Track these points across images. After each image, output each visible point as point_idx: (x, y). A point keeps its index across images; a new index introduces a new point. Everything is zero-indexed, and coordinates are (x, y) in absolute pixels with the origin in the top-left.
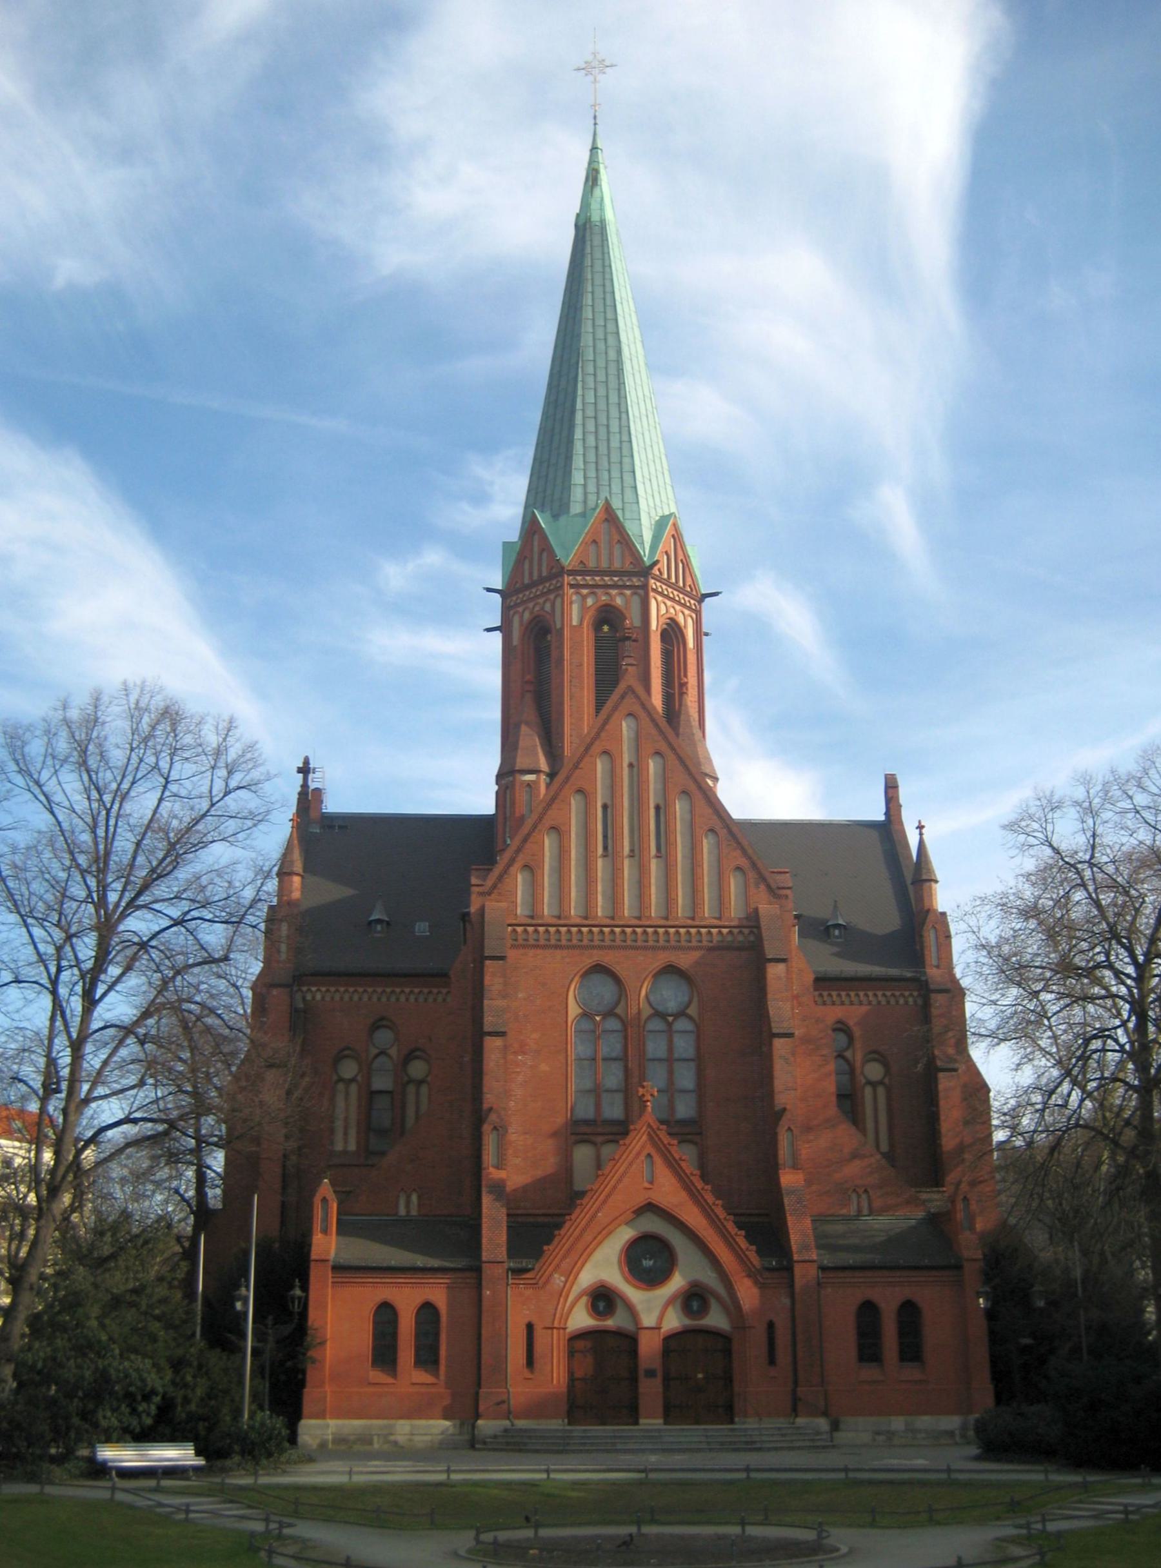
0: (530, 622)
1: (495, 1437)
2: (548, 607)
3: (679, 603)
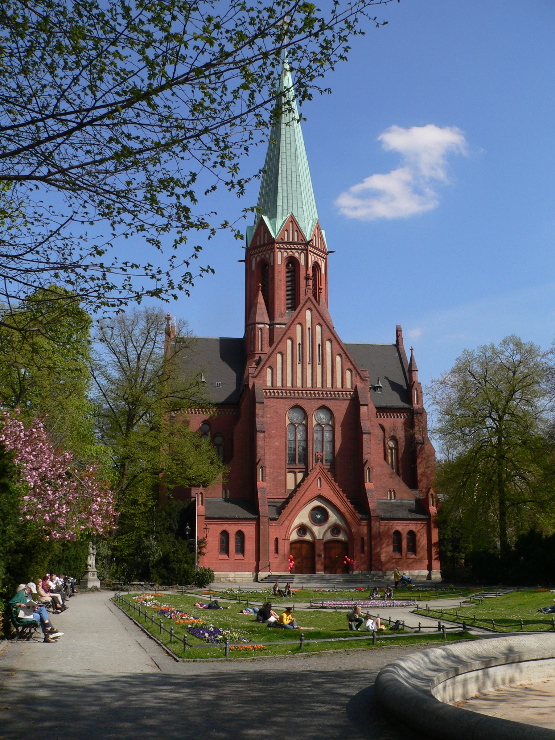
0: (260, 261)
1: (265, 578)
2: (267, 256)
3: (319, 255)
